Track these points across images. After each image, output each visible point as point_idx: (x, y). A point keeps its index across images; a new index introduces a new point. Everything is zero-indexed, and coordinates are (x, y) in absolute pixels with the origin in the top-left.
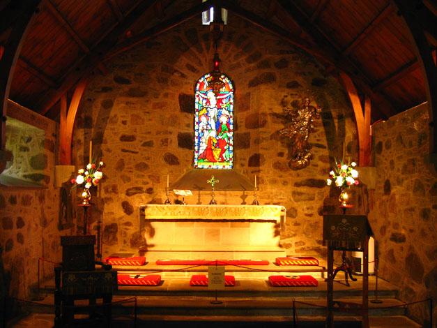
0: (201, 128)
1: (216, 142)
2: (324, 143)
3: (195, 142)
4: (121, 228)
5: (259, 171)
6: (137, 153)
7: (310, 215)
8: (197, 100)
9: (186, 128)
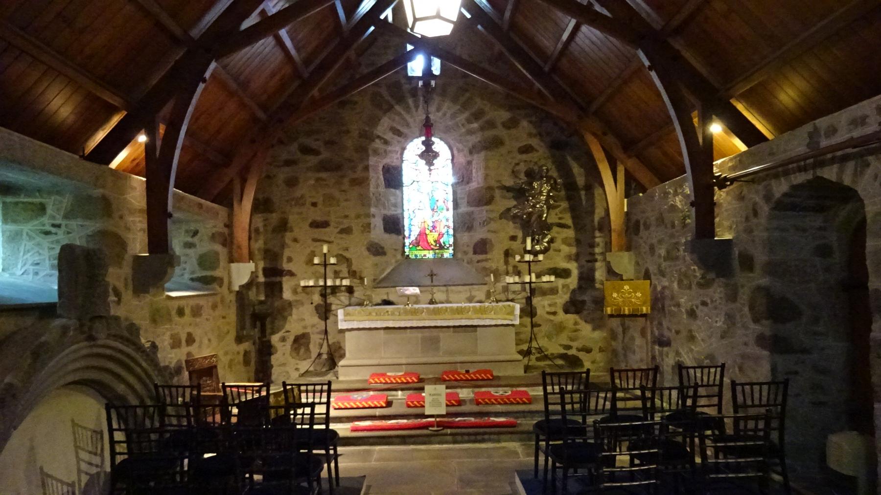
2: (569, 221)
9: (393, 208)
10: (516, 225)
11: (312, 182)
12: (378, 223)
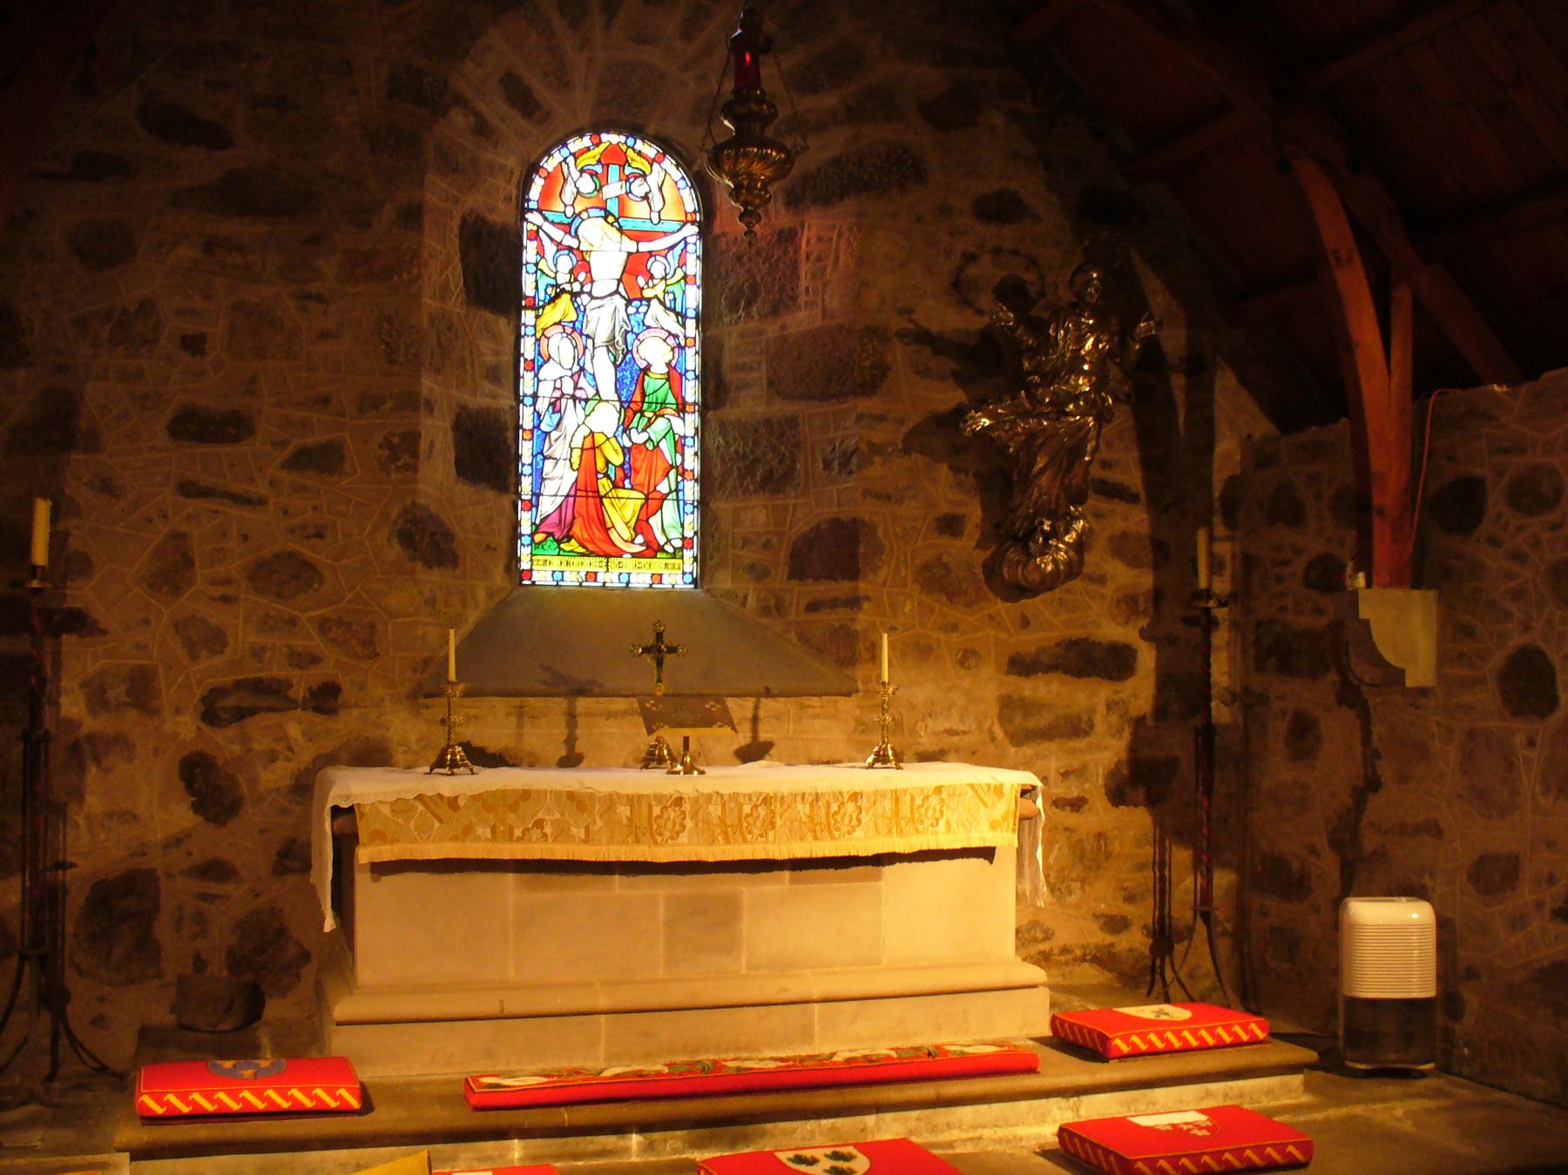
0: (546, 390)
1: (617, 459)
2: (1132, 477)
3: (518, 457)
4: (176, 892)
5: (854, 602)
6: (261, 502)
7: (1077, 805)
8: (529, 254)
9: (487, 386)
10: (962, 476)
11: (186, 253)
12: (438, 434)
